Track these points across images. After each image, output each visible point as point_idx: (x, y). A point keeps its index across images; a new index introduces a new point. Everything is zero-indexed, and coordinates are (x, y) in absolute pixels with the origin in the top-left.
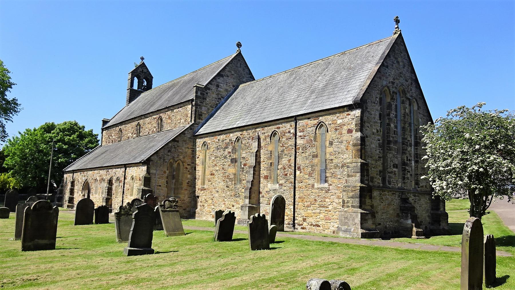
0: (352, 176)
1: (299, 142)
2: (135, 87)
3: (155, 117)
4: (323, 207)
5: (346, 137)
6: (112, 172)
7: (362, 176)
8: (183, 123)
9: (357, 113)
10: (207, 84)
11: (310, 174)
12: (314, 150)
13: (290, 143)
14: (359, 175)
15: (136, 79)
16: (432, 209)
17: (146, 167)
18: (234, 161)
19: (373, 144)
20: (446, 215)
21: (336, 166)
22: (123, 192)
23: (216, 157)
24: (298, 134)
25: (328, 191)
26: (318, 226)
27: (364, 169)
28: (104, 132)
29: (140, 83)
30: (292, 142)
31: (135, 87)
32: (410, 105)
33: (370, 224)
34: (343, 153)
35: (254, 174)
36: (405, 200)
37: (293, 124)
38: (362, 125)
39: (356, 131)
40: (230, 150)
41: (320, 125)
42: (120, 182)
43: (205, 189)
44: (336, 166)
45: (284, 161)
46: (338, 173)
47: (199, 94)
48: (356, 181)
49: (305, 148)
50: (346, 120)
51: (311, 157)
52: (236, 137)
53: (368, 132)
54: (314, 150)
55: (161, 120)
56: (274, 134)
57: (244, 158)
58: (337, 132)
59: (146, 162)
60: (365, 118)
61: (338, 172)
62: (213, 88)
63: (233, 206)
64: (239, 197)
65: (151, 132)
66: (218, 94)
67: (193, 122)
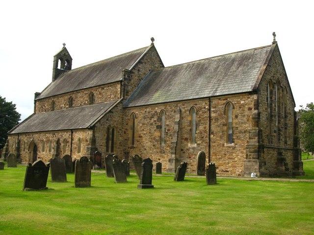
0: (252, 139)
1: (213, 115)
2: (59, 67)
3: (86, 92)
4: (231, 159)
5: (247, 112)
6: (59, 135)
7: (259, 138)
8: (113, 98)
9: (255, 97)
10: (132, 69)
11: (221, 137)
12: (224, 121)
13: (205, 115)
14: (257, 138)
15: (60, 62)
16: (294, 160)
17: (92, 132)
18: (159, 127)
19: (264, 117)
20: (302, 163)
21: (240, 132)
22: (71, 150)
23: (143, 124)
24: (212, 109)
25: (234, 148)
26: (228, 172)
27: (260, 134)
28: (37, 103)
29: (63, 63)
30: (207, 115)
31: (59, 67)
32: (282, 91)
33: (263, 169)
34: (245, 123)
35: (178, 137)
36: (280, 154)
37: (207, 102)
38: (257, 105)
39: (255, 109)
40: (156, 119)
41: (228, 104)
42: (68, 142)
43: (134, 148)
44: (240, 132)
45: (201, 128)
46: (242, 136)
47: (126, 77)
48: (254, 142)
49: (217, 119)
50: (247, 102)
51: (221, 125)
52: (160, 110)
53: (261, 110)
54: (224, 121)
55: (93, 95)
56: (192, 108)
57: (168, 125)
58: (241, 109)
59: (92, 128)
60: (260, 101)
61: (242, 136)
62: (136, 72)
63: (159, 159)
64: (164, 153)
65: (82, 104)
66: (139, 77)
67: (122, 98)
